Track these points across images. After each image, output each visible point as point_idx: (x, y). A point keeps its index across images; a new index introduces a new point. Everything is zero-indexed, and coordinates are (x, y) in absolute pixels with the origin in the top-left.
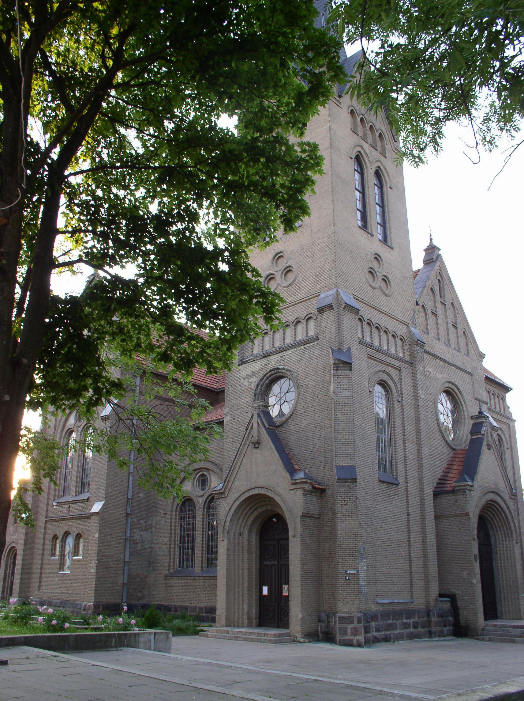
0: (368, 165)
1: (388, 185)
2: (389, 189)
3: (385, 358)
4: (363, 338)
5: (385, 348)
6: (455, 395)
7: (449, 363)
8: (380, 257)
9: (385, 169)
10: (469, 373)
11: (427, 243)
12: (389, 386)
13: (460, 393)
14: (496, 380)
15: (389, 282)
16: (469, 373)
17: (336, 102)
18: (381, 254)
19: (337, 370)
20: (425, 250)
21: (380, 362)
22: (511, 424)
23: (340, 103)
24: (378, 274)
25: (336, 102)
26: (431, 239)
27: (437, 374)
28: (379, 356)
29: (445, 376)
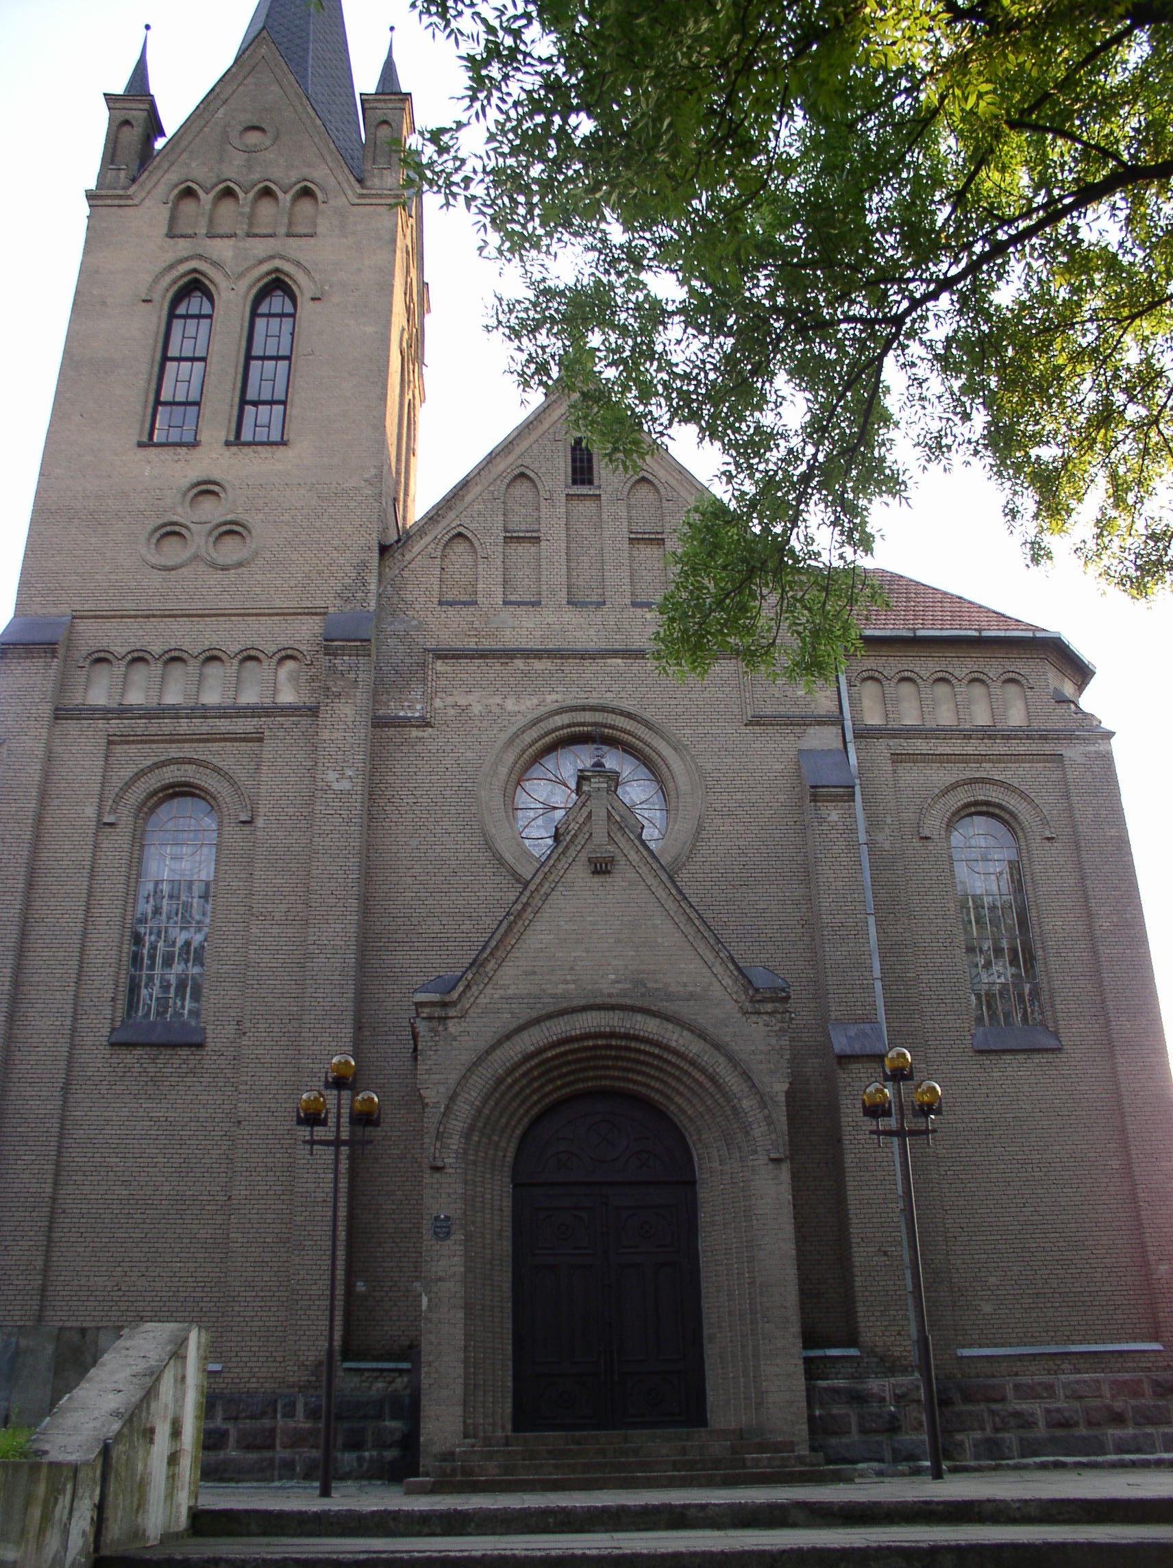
9: (298, 264)
13: (647, 724)
14: (1039, 634)
17: (116, 202)
23: (129, 197)
25: (116, 202)
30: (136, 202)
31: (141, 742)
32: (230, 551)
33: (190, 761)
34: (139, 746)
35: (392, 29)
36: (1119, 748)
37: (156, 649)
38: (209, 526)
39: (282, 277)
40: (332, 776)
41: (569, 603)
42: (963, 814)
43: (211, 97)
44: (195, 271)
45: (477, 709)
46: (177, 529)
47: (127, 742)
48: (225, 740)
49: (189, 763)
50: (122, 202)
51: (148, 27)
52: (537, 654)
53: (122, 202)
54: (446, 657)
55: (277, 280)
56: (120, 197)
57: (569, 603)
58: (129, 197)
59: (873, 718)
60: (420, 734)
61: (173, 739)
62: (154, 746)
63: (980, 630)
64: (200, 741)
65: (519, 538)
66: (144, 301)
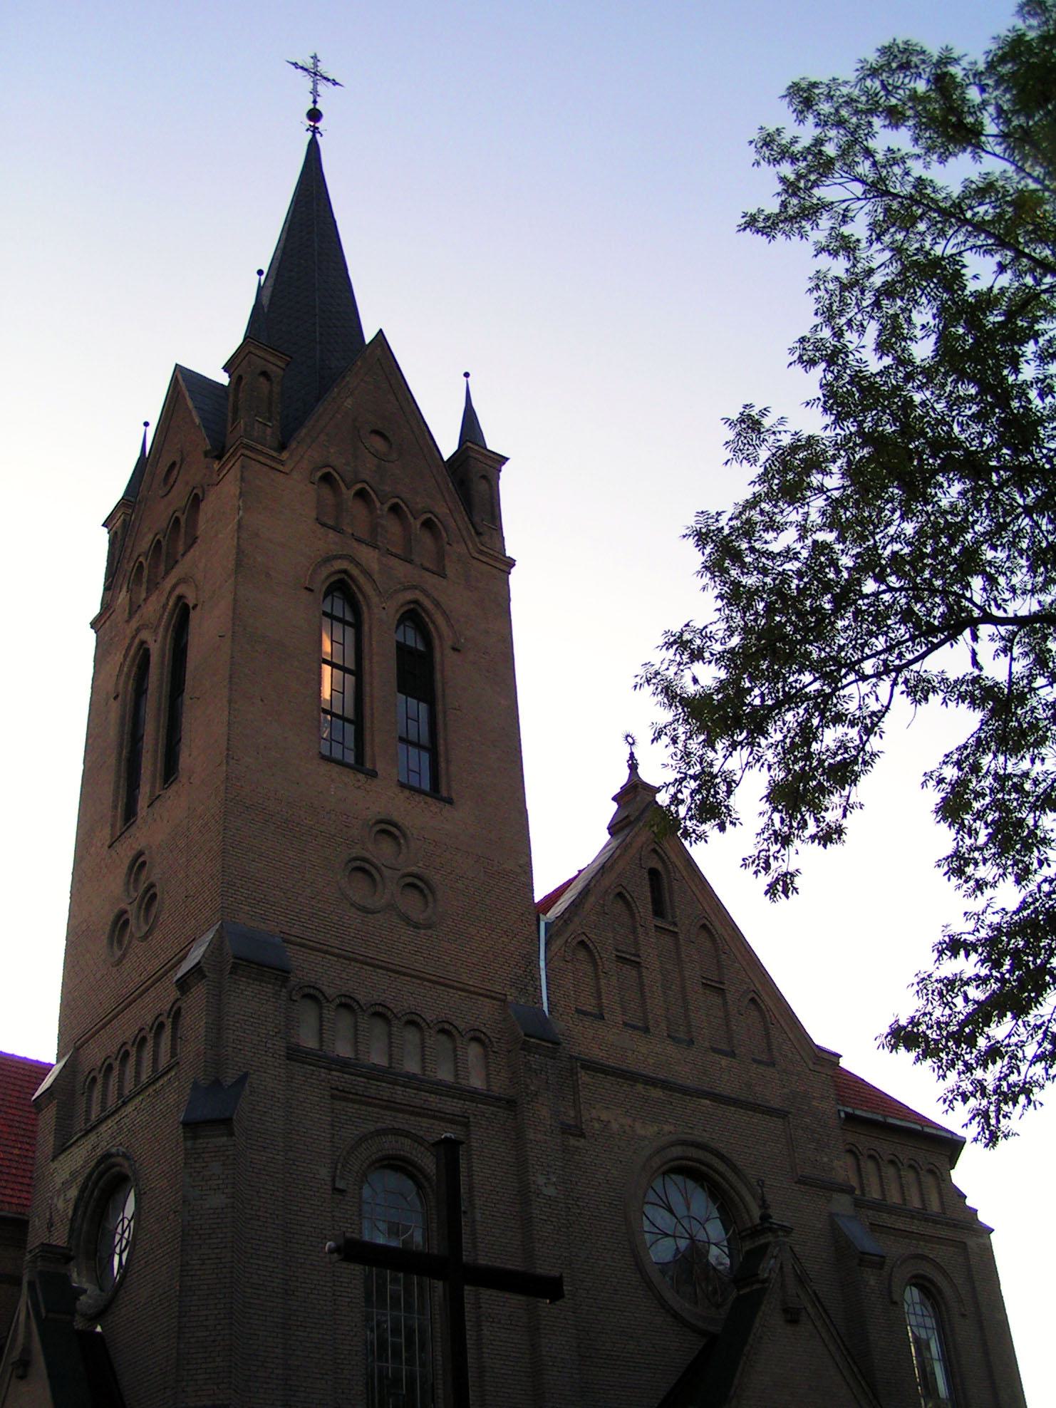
0: (375, 600)
1: (449, 643)
2: (449, 652)
3: (916, 1227)
4: (925, 1208)
5: (916, 1203)
6: (717, 1177)
7: (685, 1091)
8: (395, 825)
9: (437, 604)
10: (770, 1111)
11: (623, 776)
12: (940, 1292)
13: (735, 1169)
14: (927, 1130)
15: (433, 892)
16: (770, 1111)
17: (269, 462)
18: (396, 817)
19: (195, 1138)
20: (614, 799)
21: (386, 1108)
22: (972, 1242)
23: (282, 463)
24: (386, 872)
25: (269, 462)
26: (633, 766)
27: (638, 1125)
28: (886, 1219)
29: (667, 1128)
30: (286, 469)
31: (360, 1102)
32: (411, 904)
33: (407, 1134)
34: (357, 1106)
35: (467, 375)
36: (998, 1243)
37: (429, 1016)
38: (400, 873)
39: (420, 610)
40: (541, 1180)
41: (669, 1036)
42: (385, 1163)
43: (422, 423)
44: (345, 572)
45: (615, 1126)
46: (367, 866)
47: (346, 1099)
48: (434, 1117)
49: (406, 1137)
50: (274, 465)
51: (467, 375)
52: (651, 1082)
53: (274, 465)
54: (596, 1070)
55: (341, 581)
56: (273, 458)
57: (669, 1036)
58: (282, 463)
59: (308, 1040)
60: (577, 1144)
61: (390, 1105)
62: (370, 1109)
63: (884, 1117)
64: (412, 1113)
65: (625, 959)
66: (306, 588)
